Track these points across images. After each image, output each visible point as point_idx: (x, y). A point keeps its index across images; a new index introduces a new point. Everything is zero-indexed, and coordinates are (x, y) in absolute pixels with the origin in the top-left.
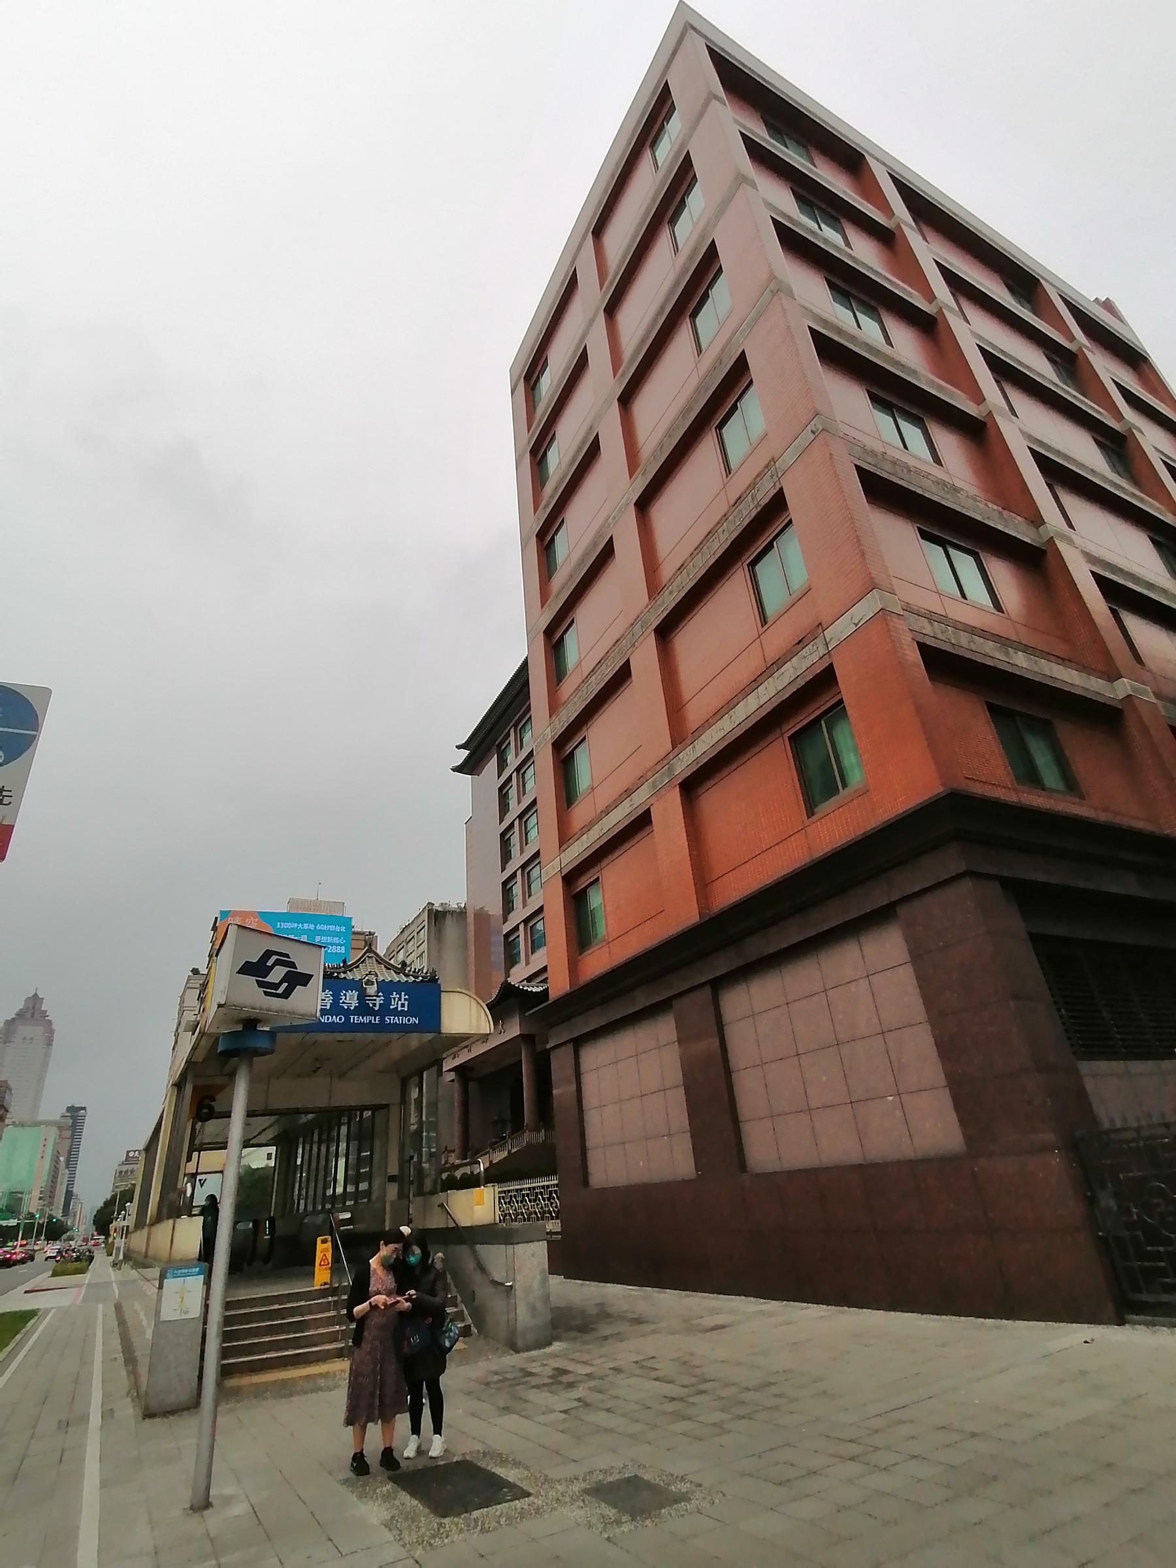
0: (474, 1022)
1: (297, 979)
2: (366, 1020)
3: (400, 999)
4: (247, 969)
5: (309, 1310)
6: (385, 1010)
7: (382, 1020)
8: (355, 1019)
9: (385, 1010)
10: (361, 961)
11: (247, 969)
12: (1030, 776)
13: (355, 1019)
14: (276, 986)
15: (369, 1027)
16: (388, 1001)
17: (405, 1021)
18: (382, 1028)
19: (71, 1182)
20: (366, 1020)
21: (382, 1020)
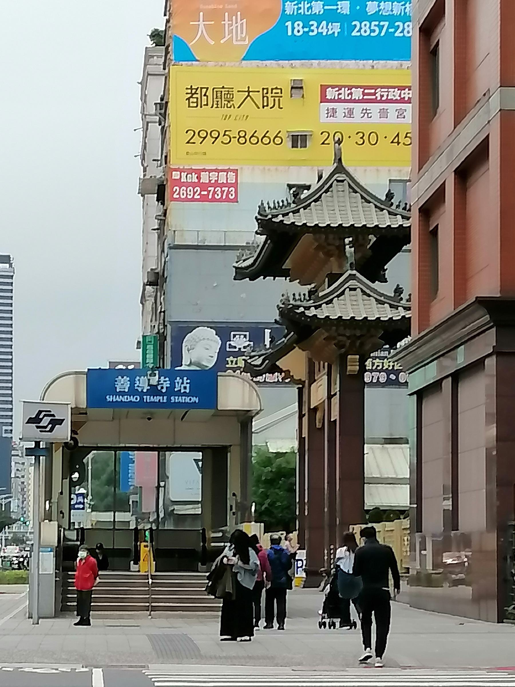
0: (247, 401)
1: (56, 422)
2: (156, 399)
3: (182, 383)
4: (31, 421)
5: (133, 584)
6: (171, 391)
7: (169, 399)
8: (148, 399)
9: (171, 391)
10: (326, 187)
11: (31, 421)
12: (335, 394)
13: (148, 399)
14: (46, 427)
15: (159, 405)
16: (173, 385)
17: (188, 400)
18: (169, 405)
19: (147, 240)
20: (156, 399)
21: (169, 399)
